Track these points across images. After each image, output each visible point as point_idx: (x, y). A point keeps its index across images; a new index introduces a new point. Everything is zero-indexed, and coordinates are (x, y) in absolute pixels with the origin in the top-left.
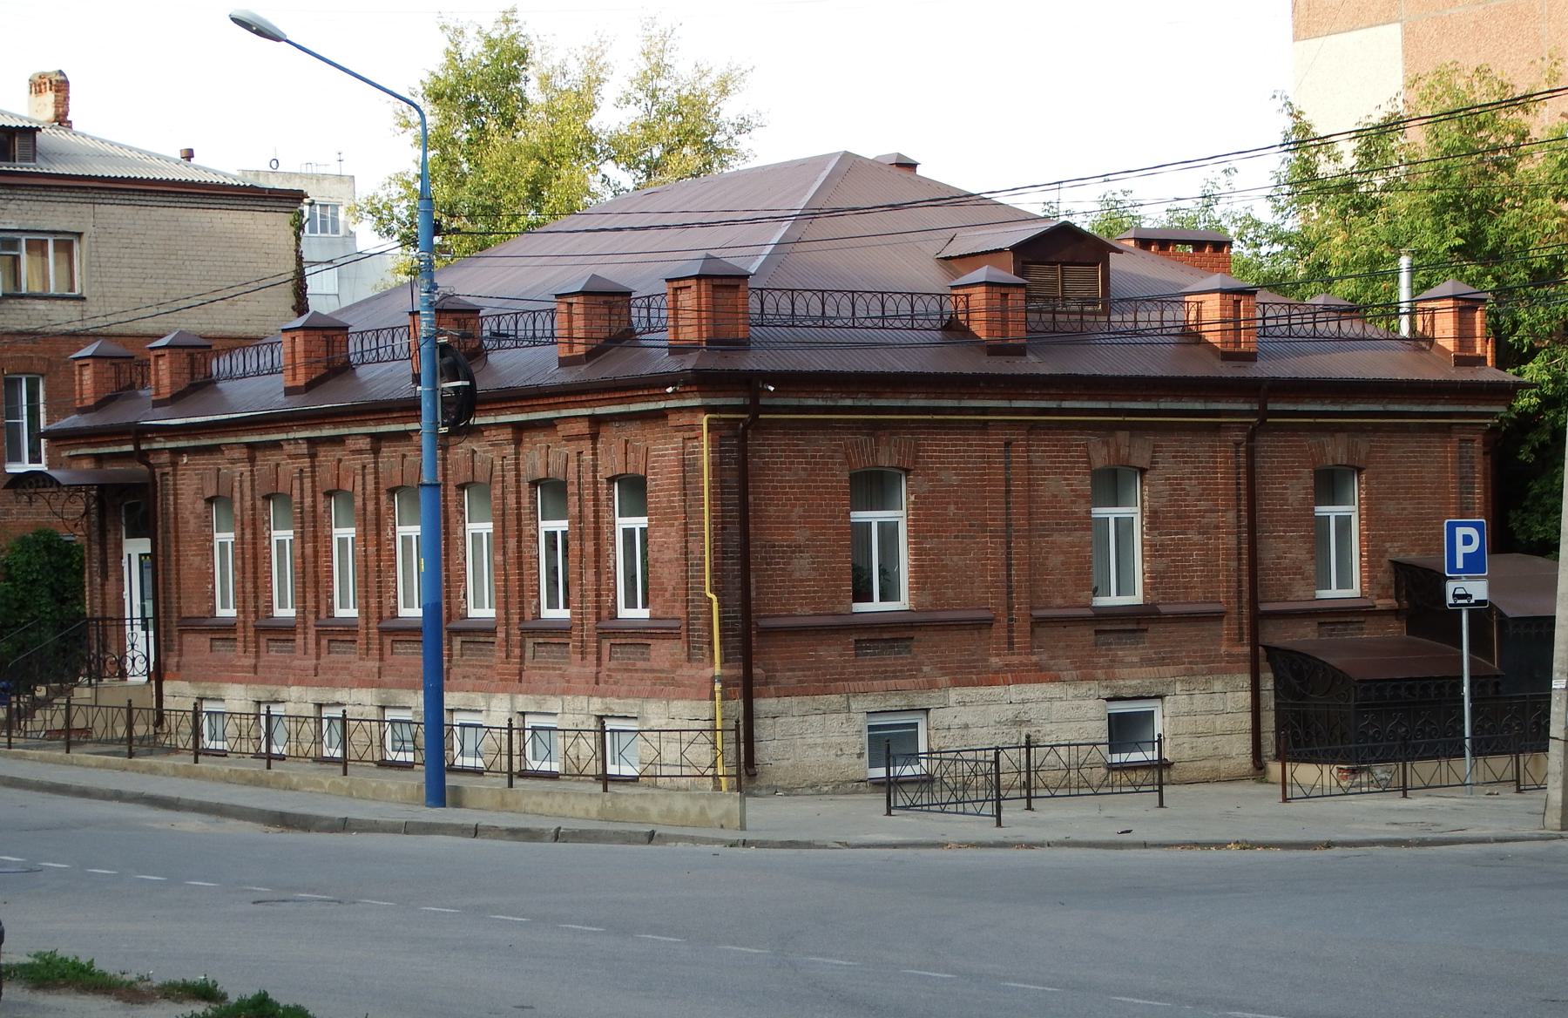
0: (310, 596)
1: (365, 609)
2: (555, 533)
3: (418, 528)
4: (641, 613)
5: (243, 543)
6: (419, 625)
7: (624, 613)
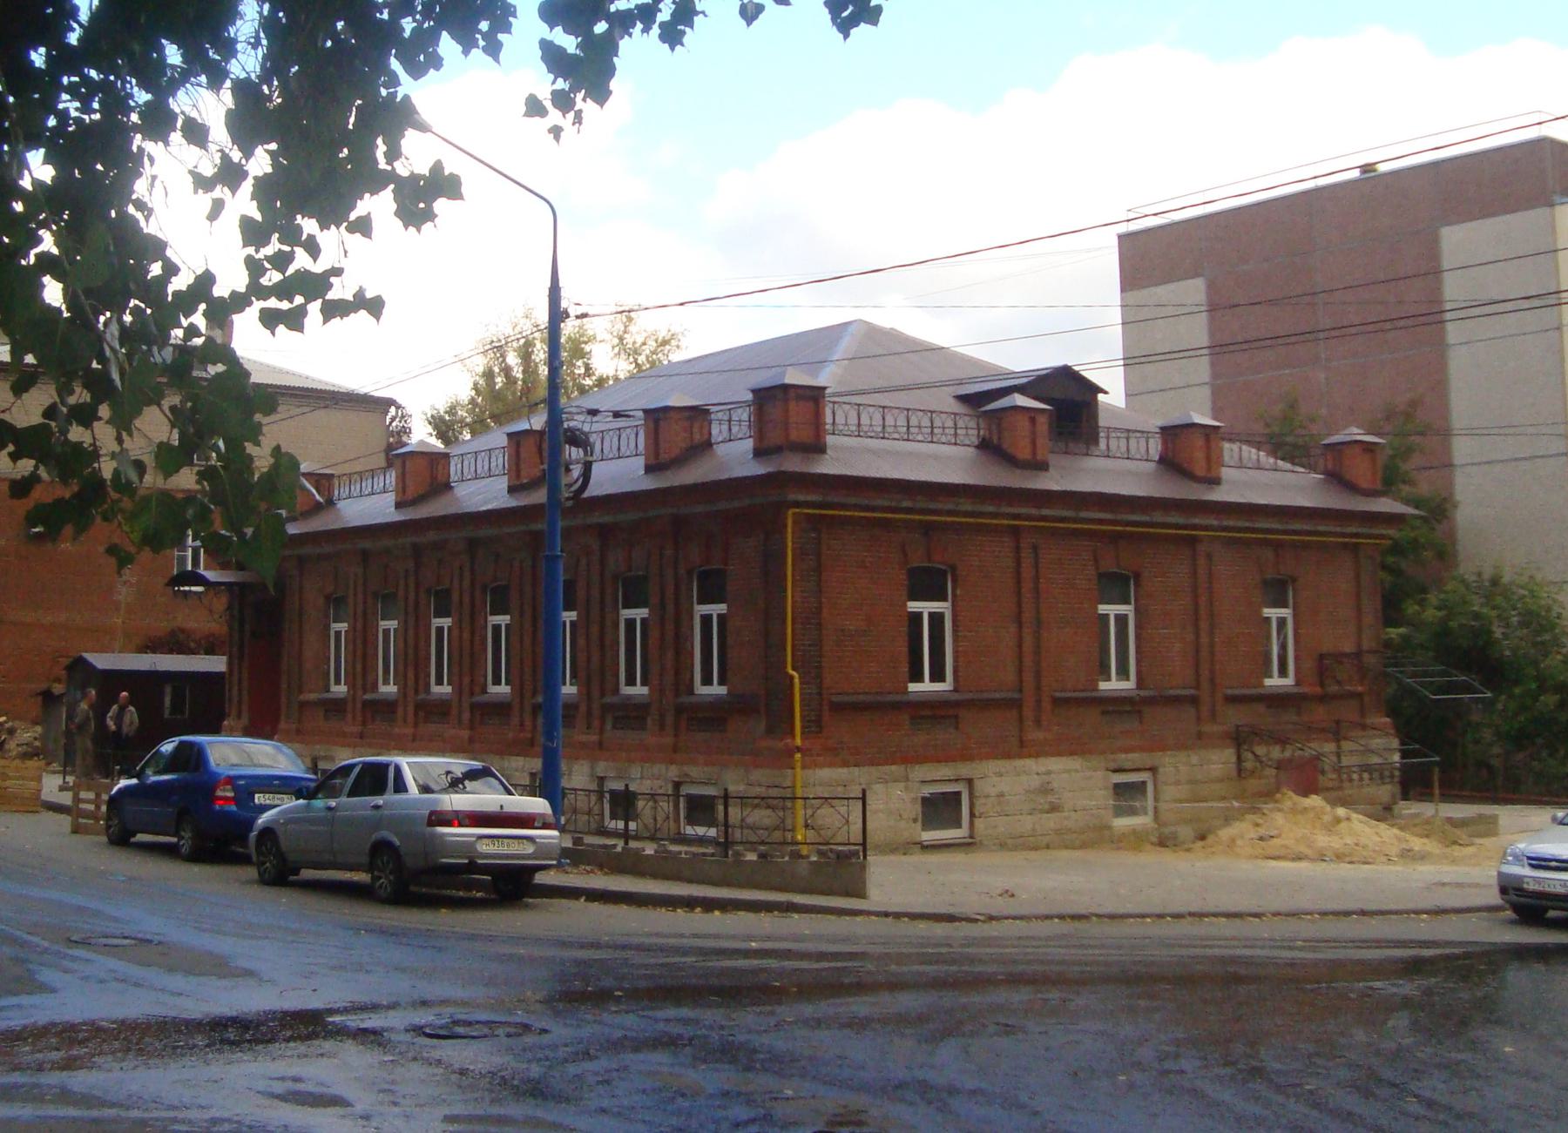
0: (411, 675)
1: (459, 690)
2: (500, 626)
3: (396, 622)
4: (718, 690)
5: (355, 631)
6: (509, 700)
7: (701, 690)
